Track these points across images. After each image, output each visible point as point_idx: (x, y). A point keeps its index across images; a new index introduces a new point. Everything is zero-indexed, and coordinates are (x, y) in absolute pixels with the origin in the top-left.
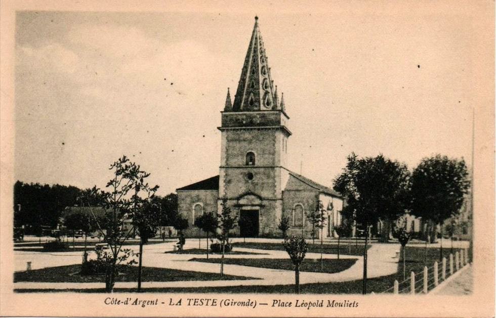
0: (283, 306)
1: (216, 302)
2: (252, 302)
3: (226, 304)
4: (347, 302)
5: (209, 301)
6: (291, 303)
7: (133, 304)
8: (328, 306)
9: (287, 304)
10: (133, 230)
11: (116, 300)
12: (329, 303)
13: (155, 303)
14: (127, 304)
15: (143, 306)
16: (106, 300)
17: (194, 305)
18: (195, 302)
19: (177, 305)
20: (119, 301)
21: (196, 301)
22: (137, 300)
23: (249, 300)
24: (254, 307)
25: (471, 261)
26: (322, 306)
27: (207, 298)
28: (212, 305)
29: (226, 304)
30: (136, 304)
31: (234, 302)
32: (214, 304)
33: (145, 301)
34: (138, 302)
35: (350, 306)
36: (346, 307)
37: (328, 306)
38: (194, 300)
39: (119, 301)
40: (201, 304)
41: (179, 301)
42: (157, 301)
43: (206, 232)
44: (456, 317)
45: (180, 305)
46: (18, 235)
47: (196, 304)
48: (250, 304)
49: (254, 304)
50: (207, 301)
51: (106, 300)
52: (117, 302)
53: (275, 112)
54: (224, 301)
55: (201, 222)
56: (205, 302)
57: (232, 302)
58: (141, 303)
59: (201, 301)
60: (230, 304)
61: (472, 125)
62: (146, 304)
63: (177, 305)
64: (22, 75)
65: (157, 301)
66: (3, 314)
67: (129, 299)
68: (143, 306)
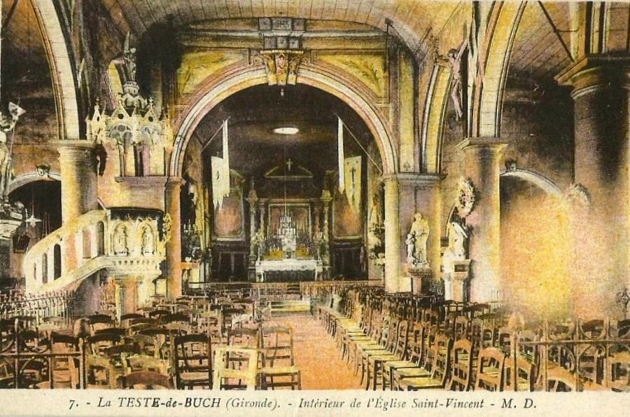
2: (271, 403)
3: (235, 404)
4: (394, 401)
5: (149, 400)
8: (503, 407)
9: (467, 405)
12: (505, 402)
13: (434, 405)
18: (154, 402)
20: (175, 402)
23: (266, 399)
24: (272, 410)
25: (613, 389)
27: (146, 397)
28: (153, 406)
29: (235, 404)
31: (244, 401)
35: (174, 406)
37: (503, 407)
38: (128, 400)
39: (175, 402)
42: (482, 402)
44: (28, 414)
46: (579, 3)
47: (130, 404)
48: (172, 404)
49: (273, 405)
52: (314, 404)
53: (427, 177)
54: (231, 401)
56: (143, 402)
57: (243, 402)
60: (240, 405)
61: (376, 278)
62: (388, 407)
67: (371, 400)
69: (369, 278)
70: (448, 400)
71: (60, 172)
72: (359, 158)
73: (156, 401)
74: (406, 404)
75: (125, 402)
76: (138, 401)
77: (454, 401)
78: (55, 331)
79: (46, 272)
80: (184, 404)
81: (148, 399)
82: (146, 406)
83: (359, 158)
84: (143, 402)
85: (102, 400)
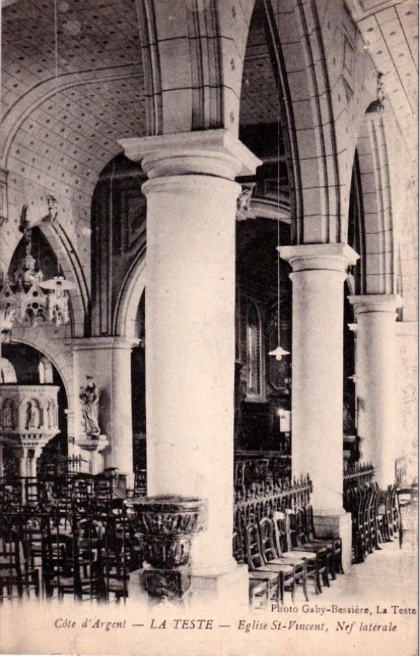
0: (366, 629)
1: (211, 624)
4: (256, 623)
6: (266, 625)
7: (93, 627)
9: (309, 627)
10: (406, 502)
11: (70, 622)
14: (85, 626)
15: (108, 629)
16: (56, 622)
17: (207, 628)
19: (160, 628)
21: (242, 623)
22: (98, 621)
26: (85, 626)
27: (201, 619)
30: (98, 627)
32: (185, 626)
33: (110, 623)
34: (100, 625)
36: (255, 630)
38: (206, 622)
40: (192, 626)
41: (162, 622)
43: (132, 506)
45: (164, 628)
50: (200, 622)
51: (56, 622)
55: (86, 488)
56: (197, 624)
58: (105, 626)
59: (194, 626)
62: (250, 628)
63: (160, 628)
64: (153, 178)
65: (125, 622)
66: (413, 646)
68: (248, 631)
69: (306, 239)
70: (291, 622)
71: (43, 281)
72: (15, 381)
73: (210, 622)
74: (397, 628)
75: (180, 624)
76: (192, 623)
77: (296, 624)
78: (104, 599)
79: (340, 225)
80: (288, 627)
81: (202, 621)
82: (200, 628)
83: (15, 381)
84: (197, 624)
85: (155, 622)
